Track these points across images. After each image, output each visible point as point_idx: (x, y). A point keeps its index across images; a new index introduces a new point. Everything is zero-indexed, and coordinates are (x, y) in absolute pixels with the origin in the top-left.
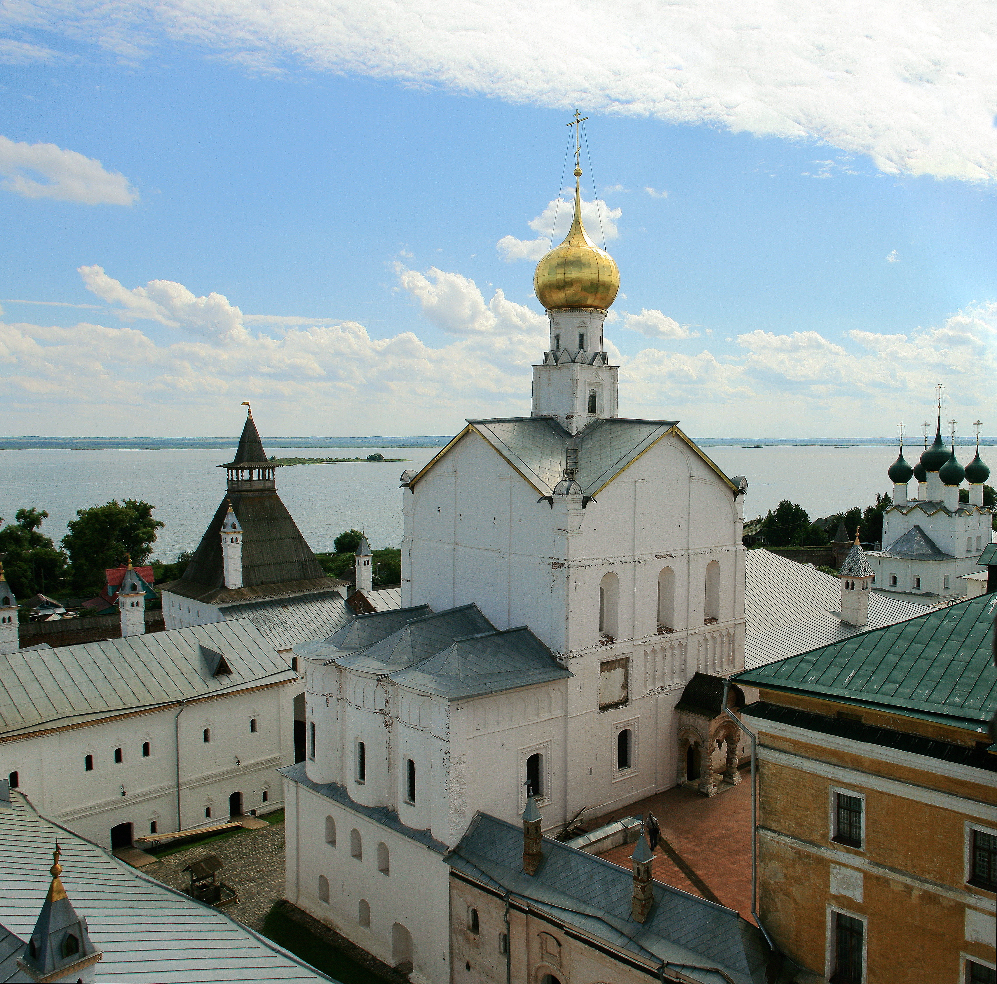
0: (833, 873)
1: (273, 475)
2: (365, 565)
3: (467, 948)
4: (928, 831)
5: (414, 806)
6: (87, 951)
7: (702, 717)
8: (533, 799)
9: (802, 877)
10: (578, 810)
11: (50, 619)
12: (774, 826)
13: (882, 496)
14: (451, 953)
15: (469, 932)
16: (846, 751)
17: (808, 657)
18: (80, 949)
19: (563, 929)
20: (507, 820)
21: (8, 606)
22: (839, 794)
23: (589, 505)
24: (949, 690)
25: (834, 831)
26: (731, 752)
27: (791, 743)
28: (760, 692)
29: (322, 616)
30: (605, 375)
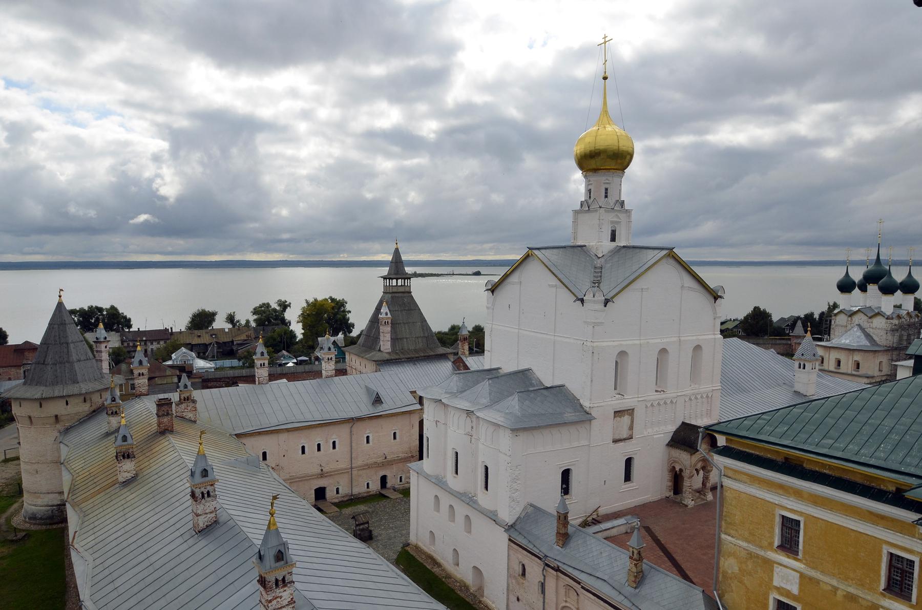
0: (776, 571)
1: (410, 283)
2: (800, 367)
3: (518, 588)
4: (853, 549)
6: (288, 562)
7: (685, 453)
8: (566, 497)
9: (752, 571)
10: (596, 507)
11: (288, 365)
12: (732, 532)
13: (831, 304)
14: (508, 590)
15: (519, 578)
16: (887, 515)
17: (764, 416)
18: (285, 559)
19: (580, 585)
20: (547, 510)
21: (899, 486)
22: (783, 516)
24: (875, 447)
25: (778, 541)
26: (706, 479)
27: (748, 476)
28: (726, 439)
30: (622, 216)
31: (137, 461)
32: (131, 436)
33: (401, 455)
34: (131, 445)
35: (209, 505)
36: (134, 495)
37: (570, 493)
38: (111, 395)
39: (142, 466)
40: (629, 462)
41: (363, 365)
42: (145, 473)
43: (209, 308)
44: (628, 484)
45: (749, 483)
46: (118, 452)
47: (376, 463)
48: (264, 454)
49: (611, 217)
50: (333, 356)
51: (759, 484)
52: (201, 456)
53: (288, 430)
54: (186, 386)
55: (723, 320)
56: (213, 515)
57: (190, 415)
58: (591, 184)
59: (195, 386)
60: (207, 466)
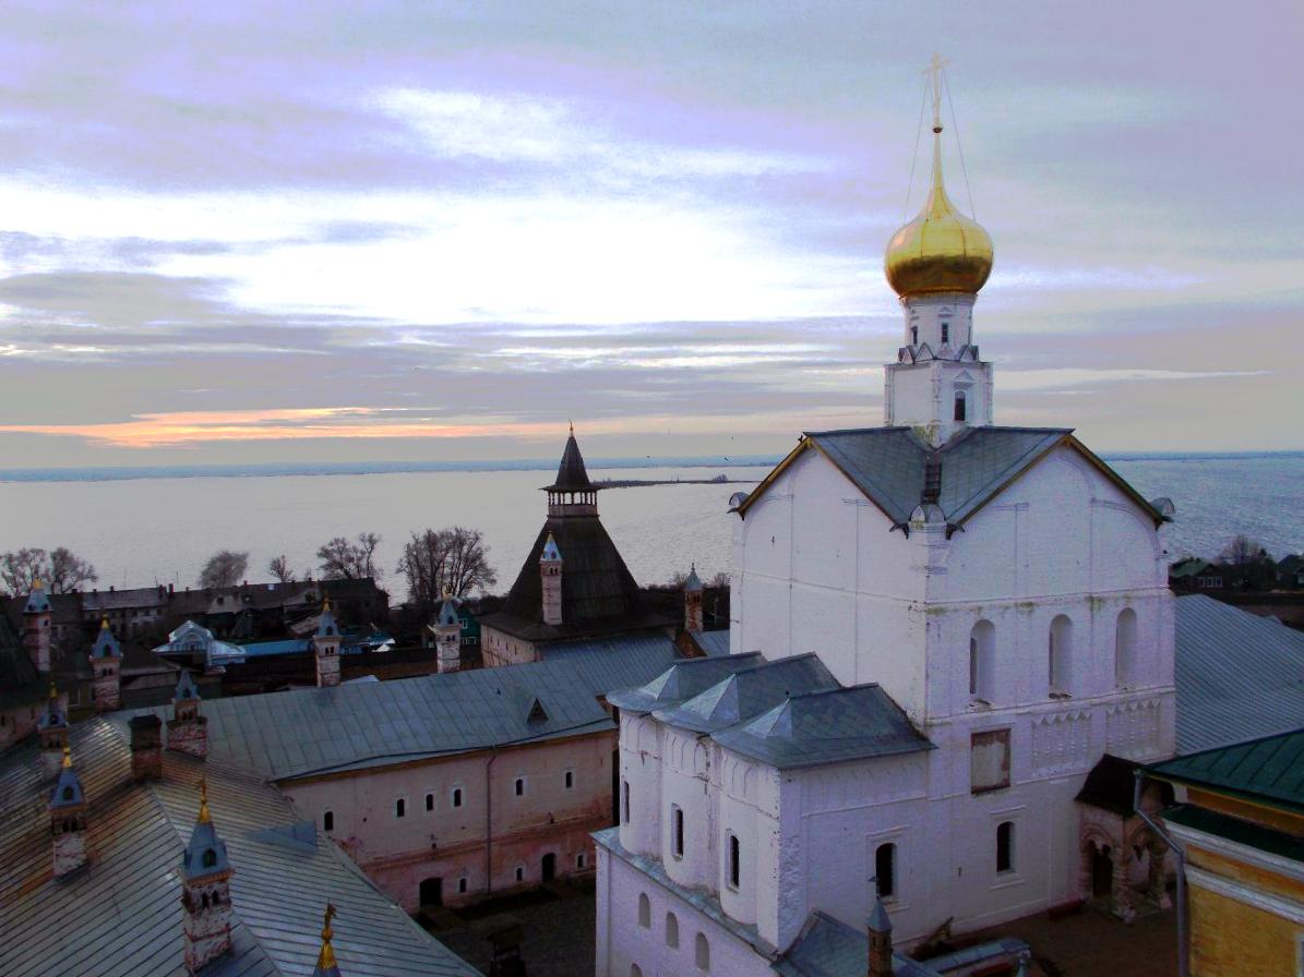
5: (736, 892)
7: (1112, 815)
8: (886, 899)
11: (380, 650)
23: (957, 535)
26: (1156, 865)
28: (1189, 791)
29: (14, 942)
30: (975, 374)
31: (88, 836)
32: (82, 789)
33: (579, 816)
34: (78, 804)
35: (217, 919)
36: (80, 901)
37: (894, 890)
38: (50, 711)
39: (98, 847)
40: (1004, 832)
41: (512, 648)
42: (103, 859)
43: (234, 548)
44: (1007, 876)
45: (1239, 878)
46: (55, 818)
47: (533, 831)
48: (329, 818)
49: (954, 375)
50: (457, 633)
51: (1259, 881)
52: (206, 826)
53: (373, 771)
54: (187, 693)
55: (1176, 559)
56: (223, 938)
57: (194, 746)
58: (917, 318)
59: (206, 692)
60: (214, 844)
